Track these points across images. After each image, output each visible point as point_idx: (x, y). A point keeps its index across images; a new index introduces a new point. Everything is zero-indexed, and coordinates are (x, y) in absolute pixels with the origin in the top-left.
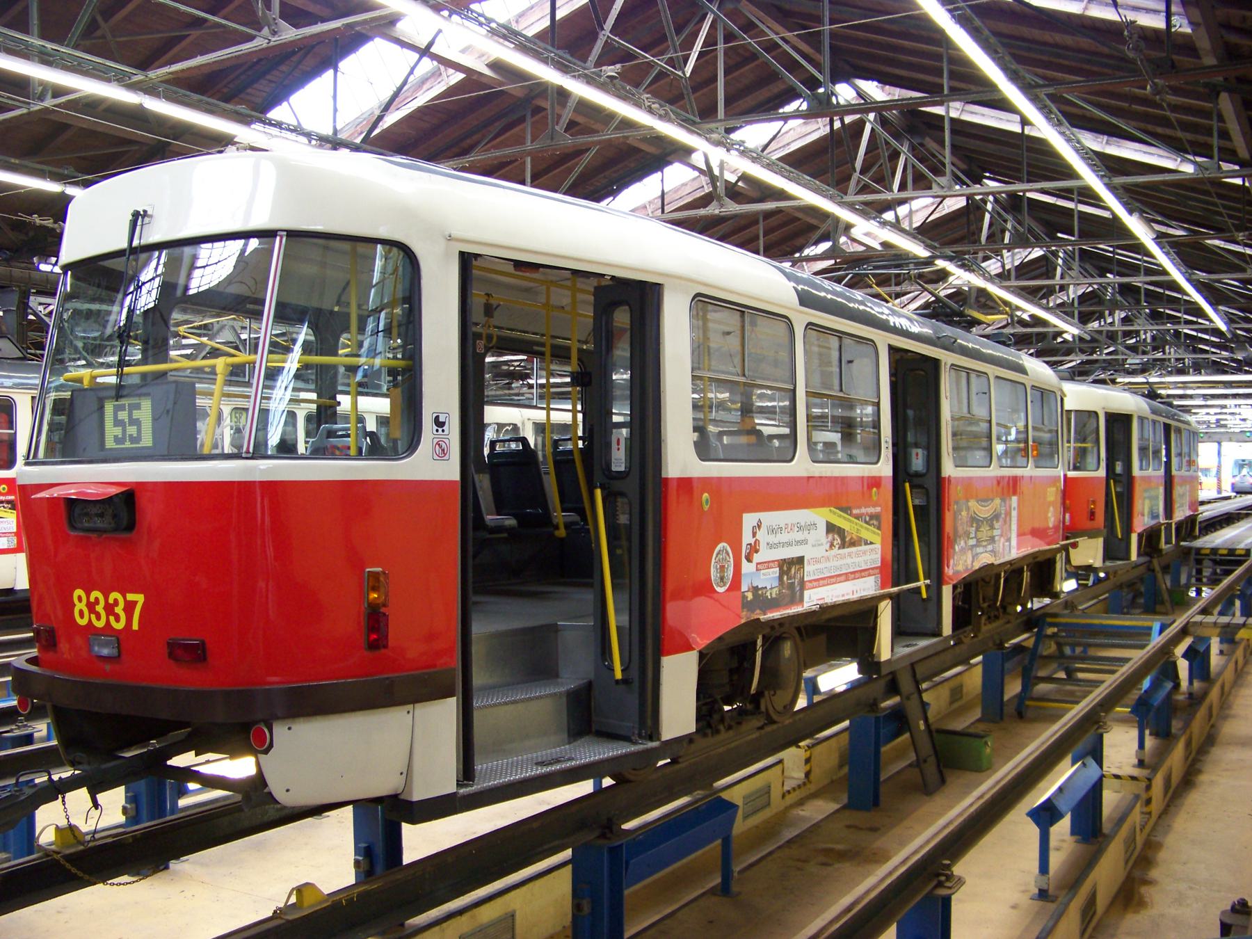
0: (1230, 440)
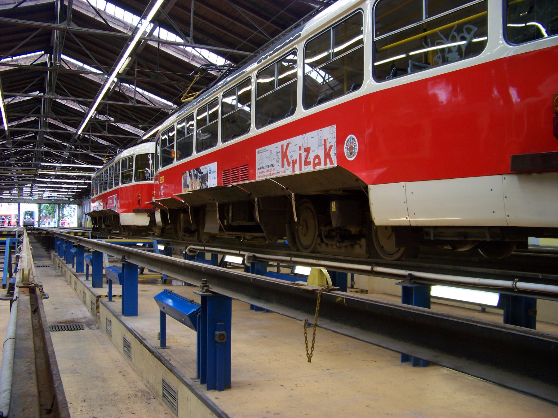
0: (24, 202)
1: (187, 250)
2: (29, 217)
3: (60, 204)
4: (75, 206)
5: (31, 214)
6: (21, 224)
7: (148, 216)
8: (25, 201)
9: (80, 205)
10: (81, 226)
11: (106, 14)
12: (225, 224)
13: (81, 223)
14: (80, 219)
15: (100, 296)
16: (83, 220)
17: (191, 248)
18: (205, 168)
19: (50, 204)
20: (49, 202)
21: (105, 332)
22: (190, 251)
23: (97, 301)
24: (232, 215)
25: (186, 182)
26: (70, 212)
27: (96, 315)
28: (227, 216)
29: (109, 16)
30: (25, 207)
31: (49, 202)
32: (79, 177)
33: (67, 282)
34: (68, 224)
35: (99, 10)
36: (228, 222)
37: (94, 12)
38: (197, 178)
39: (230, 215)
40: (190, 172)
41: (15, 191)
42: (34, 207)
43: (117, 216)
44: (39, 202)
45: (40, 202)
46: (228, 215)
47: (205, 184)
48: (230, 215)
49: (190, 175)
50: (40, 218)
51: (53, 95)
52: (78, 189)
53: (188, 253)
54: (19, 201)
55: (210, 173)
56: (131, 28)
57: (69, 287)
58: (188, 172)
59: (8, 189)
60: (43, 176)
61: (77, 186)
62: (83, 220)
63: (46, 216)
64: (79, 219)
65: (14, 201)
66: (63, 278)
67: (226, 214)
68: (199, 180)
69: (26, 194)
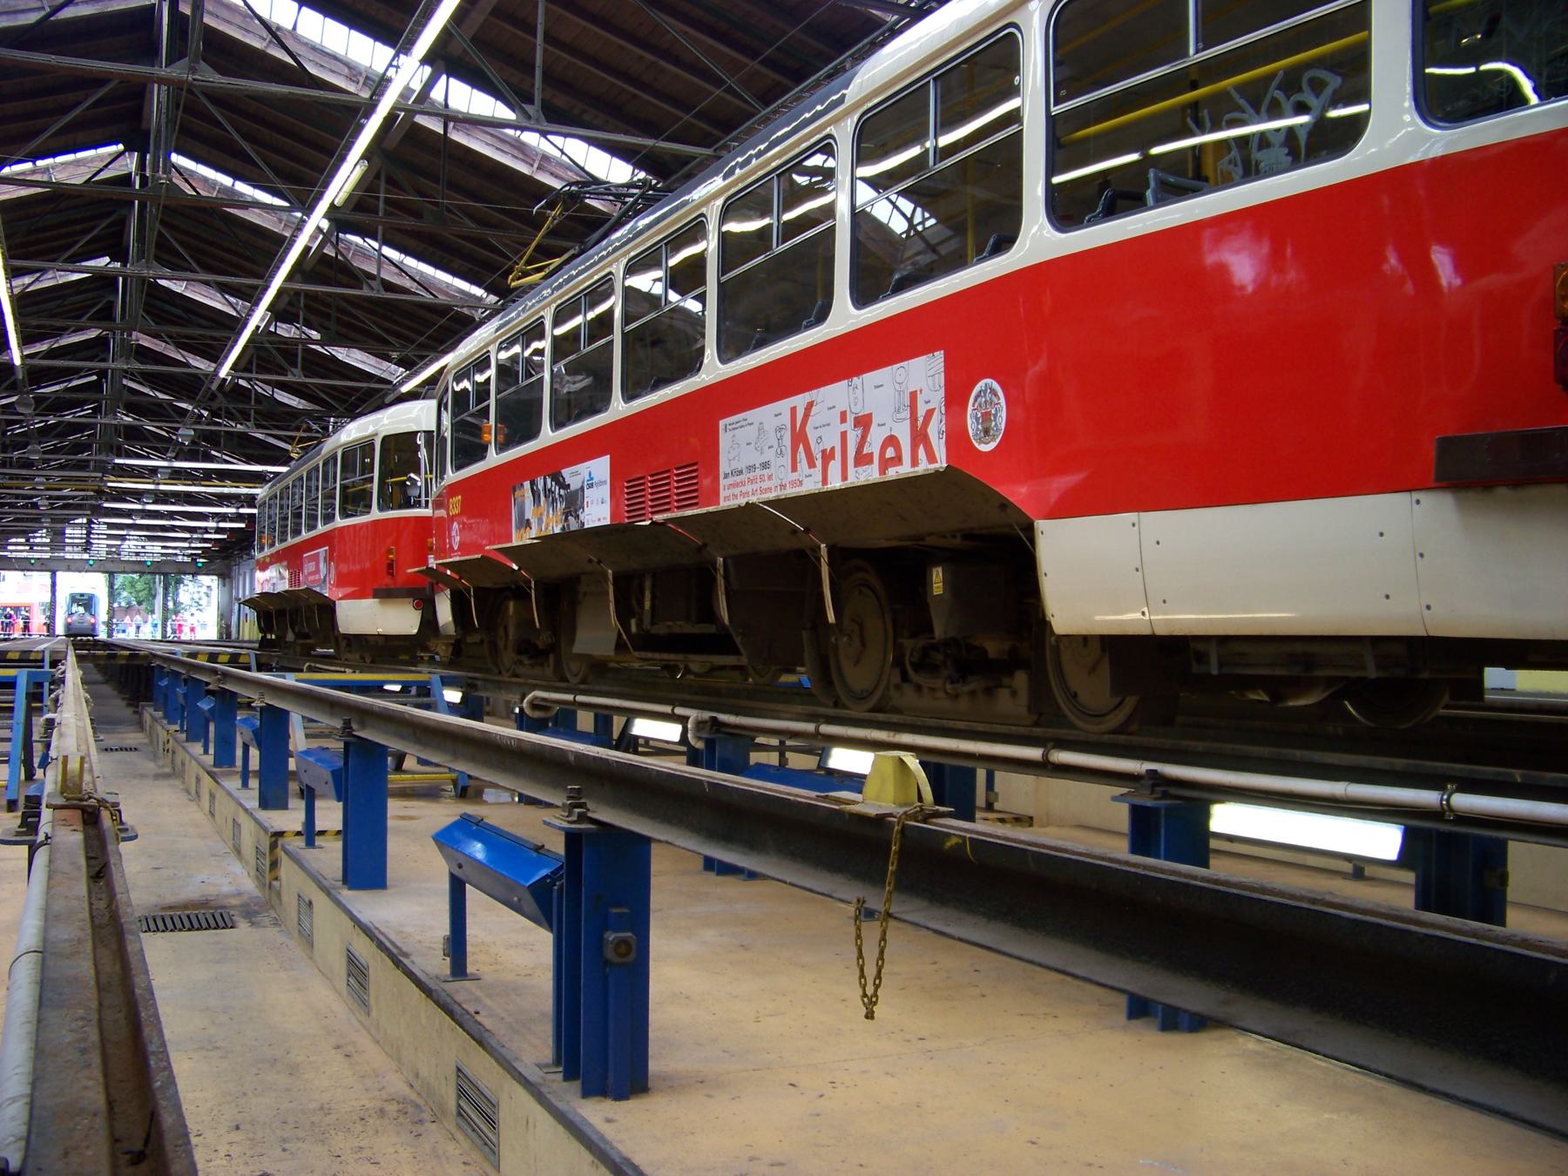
0: (69, 569)
1: (525, 704)
2: (81, 610)
3: (170, 573)
4: (210, 581)
5: (87, 602)
6: (60, 629)
7: (417, 607)
8: (72, 566)
9: (225, 576)
10: (229, 635)
11: (297, 39)
12: (634, 629)
13: (228, 627)
14: (224, 617)
15: (281, 834)
16: (234, 618)
17: (536, 698)
18: (576, 474)
19: (142, 574)
20: (137, 568)
21: (296, 934)
22: (534, 706)
23: (273, 846)
24: (653, 606)
25: (521, 513)
26: (196, 596)
27: (270, 886)
28: (636, 609)
29: (306, 44)
30: (71, 583)
31: (137, 568)
32: (222, 499)
33: (188, 792)
34: (192, 630)
35: (279, 28)
36: (639, 625)
37: (265, 33)
38: (554, 500)
39: (647, 605)
40: (533, 483)
41: (42, 537)
42: (94, 584)
43: (329, 608)
44: (111, 567)
45: (112, 567)
46: (641, 604)
47: (577, 517)
48: (647, 605)
49: (535, 493)
50: (112, 612)
51: (148, 268)
52: (219, 530)
53: (527, 711)
54: (53, 565)
55: (590, 486)
56: (367, 78)
57: (193, 807)
58: (527, 484)
59: (23, 533)
60: (122, 495)
61: (216, 524)
62: (234, 618)
63: (129, 607)
64: (222, 616)
65: (41, 566)
66: (177, 782)
67: (634, 602)
68: (561, 506)
69: (73, 545)
